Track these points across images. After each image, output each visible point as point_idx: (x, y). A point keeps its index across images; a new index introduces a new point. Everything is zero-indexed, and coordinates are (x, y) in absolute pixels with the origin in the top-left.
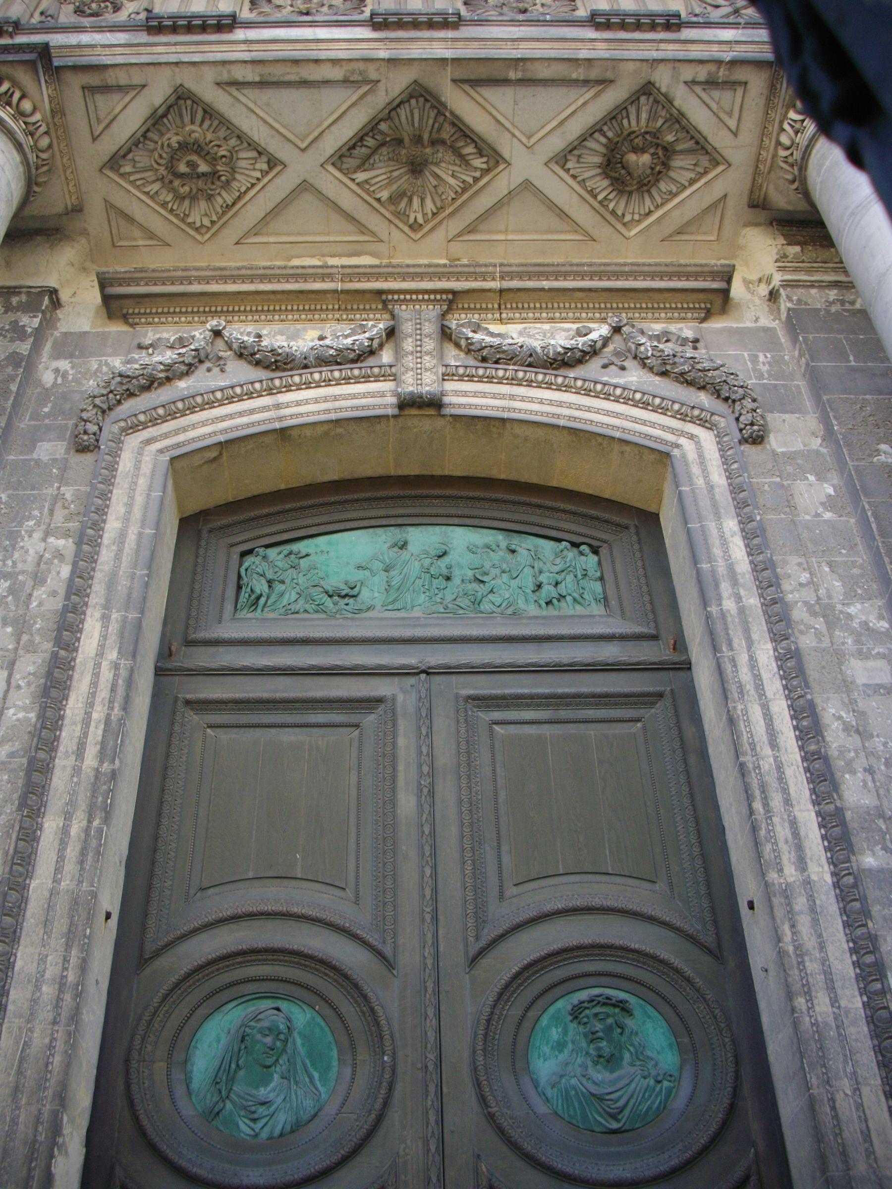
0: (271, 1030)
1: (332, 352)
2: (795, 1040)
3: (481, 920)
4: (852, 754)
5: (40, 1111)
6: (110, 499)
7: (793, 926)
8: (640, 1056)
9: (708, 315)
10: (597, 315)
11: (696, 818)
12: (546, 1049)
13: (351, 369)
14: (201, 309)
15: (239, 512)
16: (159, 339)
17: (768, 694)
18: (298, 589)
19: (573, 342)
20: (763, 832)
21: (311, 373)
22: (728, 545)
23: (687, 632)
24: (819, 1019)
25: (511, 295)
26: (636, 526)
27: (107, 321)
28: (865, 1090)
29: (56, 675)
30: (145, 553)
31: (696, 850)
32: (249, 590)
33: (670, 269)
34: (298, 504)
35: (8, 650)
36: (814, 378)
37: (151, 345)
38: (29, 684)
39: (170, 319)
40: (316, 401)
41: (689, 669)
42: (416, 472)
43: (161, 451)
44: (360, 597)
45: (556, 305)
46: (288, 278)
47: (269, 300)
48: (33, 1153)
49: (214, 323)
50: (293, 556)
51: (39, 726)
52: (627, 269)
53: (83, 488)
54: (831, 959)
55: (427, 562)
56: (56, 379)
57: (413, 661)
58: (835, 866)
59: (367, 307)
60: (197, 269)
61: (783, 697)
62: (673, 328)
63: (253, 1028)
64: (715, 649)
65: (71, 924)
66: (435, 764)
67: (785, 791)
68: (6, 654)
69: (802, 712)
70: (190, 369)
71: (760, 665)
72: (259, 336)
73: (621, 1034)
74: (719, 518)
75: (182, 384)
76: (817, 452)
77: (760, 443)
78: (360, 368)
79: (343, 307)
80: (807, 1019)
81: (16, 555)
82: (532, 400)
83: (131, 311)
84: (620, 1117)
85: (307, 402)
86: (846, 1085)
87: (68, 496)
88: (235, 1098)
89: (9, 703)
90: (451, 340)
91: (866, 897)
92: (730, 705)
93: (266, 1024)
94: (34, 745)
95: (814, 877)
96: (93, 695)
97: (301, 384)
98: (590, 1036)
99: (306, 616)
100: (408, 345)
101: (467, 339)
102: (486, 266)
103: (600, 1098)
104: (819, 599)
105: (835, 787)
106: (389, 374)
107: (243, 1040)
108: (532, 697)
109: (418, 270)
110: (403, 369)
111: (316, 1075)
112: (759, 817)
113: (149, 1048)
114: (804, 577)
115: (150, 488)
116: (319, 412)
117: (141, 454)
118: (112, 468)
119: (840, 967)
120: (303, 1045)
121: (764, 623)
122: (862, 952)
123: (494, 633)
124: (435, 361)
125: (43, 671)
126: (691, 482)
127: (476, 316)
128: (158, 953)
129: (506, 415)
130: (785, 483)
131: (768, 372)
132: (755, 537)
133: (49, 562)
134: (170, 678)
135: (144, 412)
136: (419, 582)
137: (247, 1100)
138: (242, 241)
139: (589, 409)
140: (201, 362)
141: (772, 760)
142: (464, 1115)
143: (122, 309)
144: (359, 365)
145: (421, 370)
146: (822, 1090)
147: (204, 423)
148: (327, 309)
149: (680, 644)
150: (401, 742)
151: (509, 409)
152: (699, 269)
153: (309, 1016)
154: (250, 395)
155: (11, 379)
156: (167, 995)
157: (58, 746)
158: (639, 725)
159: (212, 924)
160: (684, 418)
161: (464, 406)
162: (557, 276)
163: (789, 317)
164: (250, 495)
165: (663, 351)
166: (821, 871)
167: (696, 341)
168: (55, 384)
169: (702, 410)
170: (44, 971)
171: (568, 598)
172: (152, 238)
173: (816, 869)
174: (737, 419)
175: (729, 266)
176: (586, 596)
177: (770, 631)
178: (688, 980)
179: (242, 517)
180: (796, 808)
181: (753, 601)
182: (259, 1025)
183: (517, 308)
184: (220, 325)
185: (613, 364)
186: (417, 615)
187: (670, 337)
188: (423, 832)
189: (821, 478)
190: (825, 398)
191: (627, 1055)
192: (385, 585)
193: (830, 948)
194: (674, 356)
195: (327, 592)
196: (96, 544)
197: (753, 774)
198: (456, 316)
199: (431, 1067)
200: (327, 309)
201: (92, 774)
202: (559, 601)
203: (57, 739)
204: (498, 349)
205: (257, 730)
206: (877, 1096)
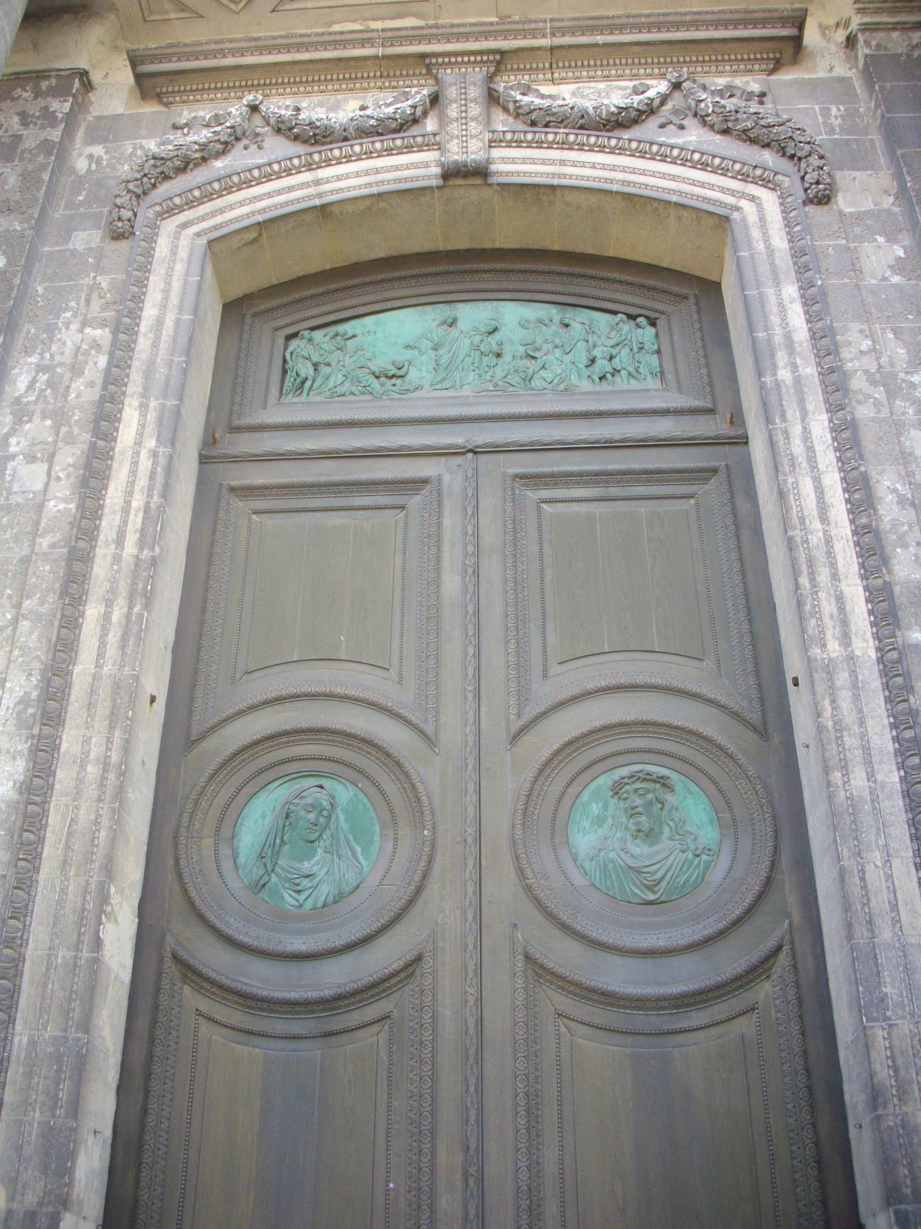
0: (315, 807)
1: (372, 122)
2: (830, 814)
3: (523, 696)
4: (906, 528)
5: (87, 883)
6: (146, 286)
7: (833, 701)
8: (680, 831)
9: (778, 66)
10: (656, 71)
11: (746, 595)
12: (586, 824)
13: (393, 139)
14: (237, 84)
15: (286, 292)
16: (195, 118)
17: (820, 466)
18: (344, 372)
19: (628, 101)
20: (808, 608)
21: (352, 146)
22: (786, 312)
23: (745, 405)
24: (855, 793)
25: (563, 53)
26: (696, 296)
27: (142, 102)
28: (896, 862)
29: (94, 465)
30: (183, 340)
31: (745, 627)
32: (294, 374)
33: (736, 17)
34: (344, 284)
35: (47, 443)
36: (890, 131)
37: (186, 125)
38: (68, 476)
39: (205, 96)
40: (357, 175)
41: (746, 443)
42: (467, 246)
43: (198, 235)
44: (408, 377)
45: (611, 62)
46: (325, 45)
47: (308, 70)
48: (82, 920)
49: (251, 97)
50: (339, 338)
51: (78, 516)
52: (688, 18)
53: (119, 277)
54: (870, 735)
55: (477, 339)
56: (90, 165)
57: (460, 441)
58: (880, 641)
59: (411, 72)
60: (230, 41)
61: (836, 469)
62: (739, 81)
63: (297, 805)
64: (768, 420)
65: (114, 706)
66: (481, 543)
67: (833, 565)
68: (46, 447)
69: (854, 485)
70: (226, 148)
71: (814, 437)
72: (298, 110)
73: (662, 809)
74: (779, 284)
75: (218, 164)
76: (888, 212)
77: (826, 203)
78: (403, 138)
79: (385, 74)
80: (843, 793)
81: (54, 348)
82: (583, 165)
83: (164, 90)
84: (656, 889)
85: (347, 176)
86: (877, 857)
87: (104, 285)
88: (281, 872)
89: (50, 494)
90: (499, 104)
91: (909, 673)
92: (781, 478)
93: (309, 801)
94: (74, 535)
95: (858, 653)
96: (132, 483)
97: (341, 158)
98: (630, 811)
99: (352, 398)
100: (453, 111)
101: (515, 102)
102: (536, 22)
103: (637, 871)
104: (880, 367)
105: (886, 561)
106: (433, 143)
107: (287, 818)
108: (580, 474)
109: (463, 30)
110: (447, 137)
111: (359, 849)
112: (805, 592)
113: (197, 825)
114: (866, 344)
115: (187, 273)
116: (360, 187)
117: (178, 239)
118: (149, 254)
119: (878, 742)
120: (346, 821)
121: (820, 394)
122: (902, 727)
123: (544, 410)
124: (481, 127)
125: (82, 462)
126: (750, 246)
127: (527, 77)
128: (204, 735)
129: (555, 182)
130: (852, 246)
131: (840, 126)
132: (815, 302)
133: (87, 354)
134: (211, 466)
135: (179, 195)
136: (469, 360)
137: (291, 873)
138: (279, 8)
139: (644, 173)
140: (238, 139)
141: (821, 534)
142: (502, 887)
143: (155, 88)
144: (402, 135)
145: (466, 137)
146: (853, 862)
147: (241, 204)
148: (368, 77)
149: (737, 418)
150: (447, 522)
151: (560, 176)
152: (767, 15)
153: (351, 793)
154: (288, 172)
155: (43, 167)
156: (214, 775)
157: (98, 536)
158: (692, 501)
159: (257, 706)
160: (745, 178)
161: (512, 173)
162: (612, 29)
163: (866, 65)
164: (294, 276)
165: (724, 107)
166: (865, 647)
167: (763, 95)
168: (89, 170)
169: (765, 169)
170: (89, 752)
171: (623, 373)
172: (183, 10)
173: (861, 645)
174: (803, 178)
175: (801, 9)
176: (641, 370)
177: (826, 401)
178: (731, 756)
179: (285, 300)
180: (843, 583)
181: (810, 370)
182: (303, 802)
183: (570, 66)
184: (257, 99)
185: (671, 123)
186: (466, 394)
187: (735, 92)
188: (467, 612)
189: (891, 239)
190: (899, 152)
191: (666, 830)
192: (434, 364)
193: (870, 723)
194: (737, 112)
195: (373, 374)
196: (132, 331)
197: (801, 549)
198: (505, 78)
199: (470, 840)
200: (368, 77)
201: (132, 561)
202: (613, 375)
203: (97, 528)
204: (548, 111)
205: (303, 514)
206: (908, 867)
